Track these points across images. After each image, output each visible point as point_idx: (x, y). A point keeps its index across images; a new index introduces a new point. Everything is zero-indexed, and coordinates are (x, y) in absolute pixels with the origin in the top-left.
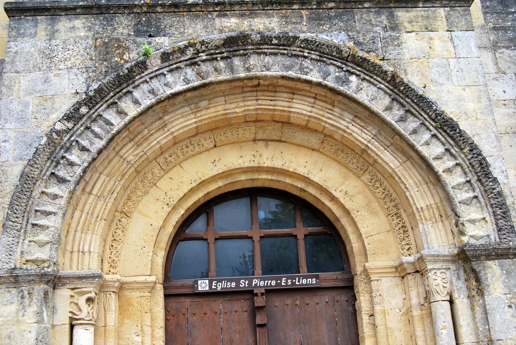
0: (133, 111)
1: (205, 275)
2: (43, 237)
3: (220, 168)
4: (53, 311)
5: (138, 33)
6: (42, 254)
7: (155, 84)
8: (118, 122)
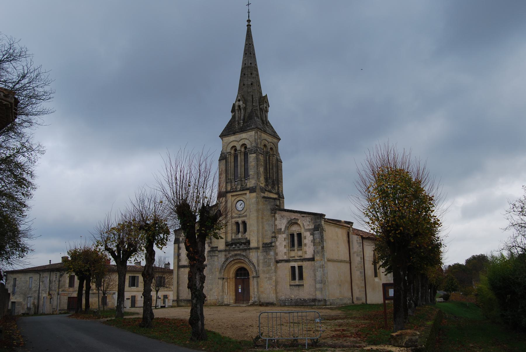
0: (228, 262)
1: (238, 277)
2: (222, 275)
3: (238, 266)
4: (223, 281)
5: (228, 254)
6: (222, 276)
7: (230, 259)
8: (227, 264)
